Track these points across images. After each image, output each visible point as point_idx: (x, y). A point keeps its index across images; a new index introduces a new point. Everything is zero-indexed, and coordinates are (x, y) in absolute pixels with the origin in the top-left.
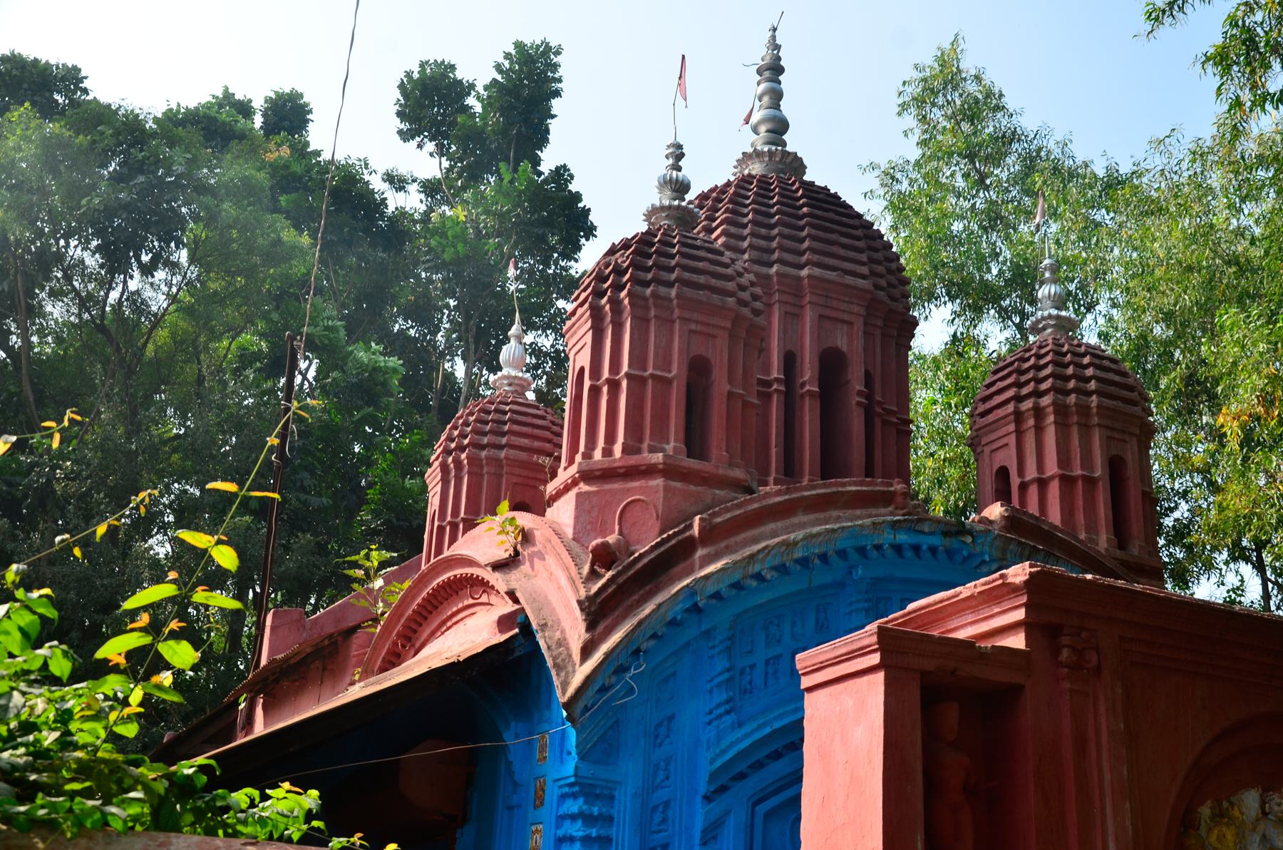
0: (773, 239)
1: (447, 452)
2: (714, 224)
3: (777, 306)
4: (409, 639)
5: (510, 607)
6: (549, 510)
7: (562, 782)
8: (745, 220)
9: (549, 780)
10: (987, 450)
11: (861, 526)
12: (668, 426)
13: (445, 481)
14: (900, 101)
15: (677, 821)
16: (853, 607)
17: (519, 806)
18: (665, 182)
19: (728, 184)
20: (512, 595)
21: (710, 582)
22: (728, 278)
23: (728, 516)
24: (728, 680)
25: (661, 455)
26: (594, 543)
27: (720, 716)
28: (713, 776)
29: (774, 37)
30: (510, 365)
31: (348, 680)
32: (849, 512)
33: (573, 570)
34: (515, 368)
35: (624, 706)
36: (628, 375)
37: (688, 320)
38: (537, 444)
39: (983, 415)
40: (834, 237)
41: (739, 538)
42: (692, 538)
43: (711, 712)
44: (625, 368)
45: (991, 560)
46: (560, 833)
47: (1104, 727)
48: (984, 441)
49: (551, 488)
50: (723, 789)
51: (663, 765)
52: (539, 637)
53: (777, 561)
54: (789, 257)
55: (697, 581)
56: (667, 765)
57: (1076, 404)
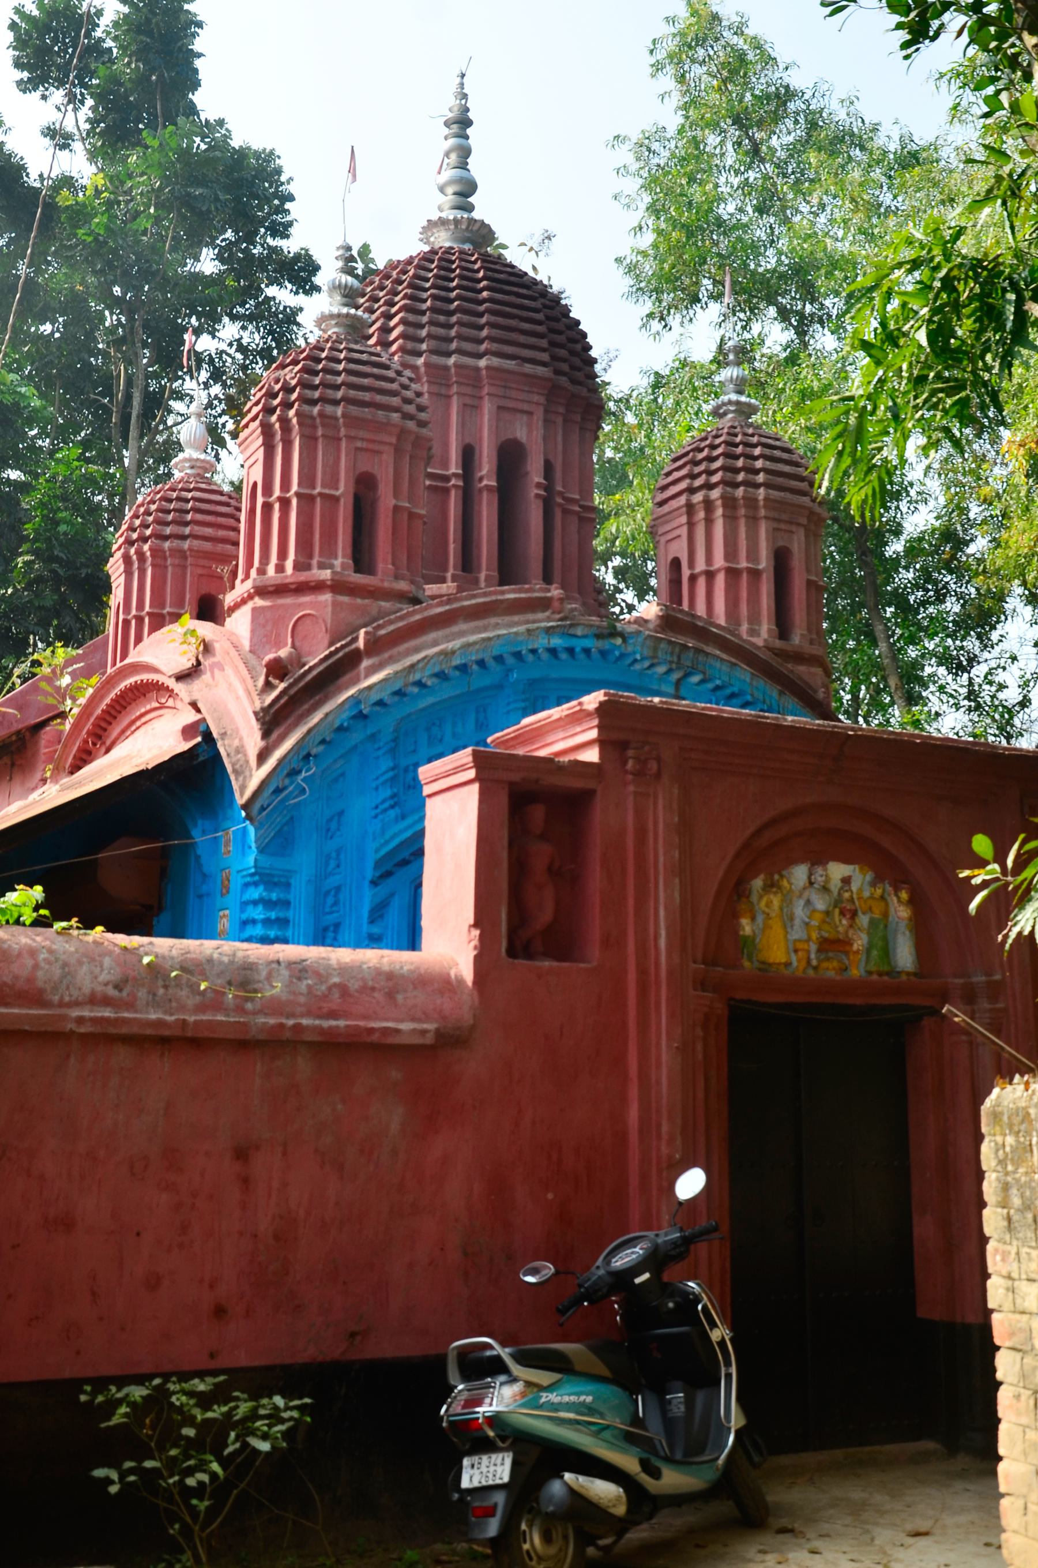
1: (130, 542)
2: (394, 310)
3: (455, 398)
4: (100, 737)
5: (192, 717)
6: (228, 620)
8: (424, 306)
10: (663, 539)
11: (516, 633)
12: (336, 542)
13: (128, 573)
14: (653, 61)
17: (208, 894)
19: (409, 261)
20: (194, 705)
21: (374, 690)
22: (394, 394)
23: (392, 628)
24: (393, 779)
25: (329, 571)
27: (385, 810)
28: (378, 864)
29: (462, 85)
31: (38, 776)
32: (507, 619)
33: (250, 682)
35: (299, 803)
36: (297, 494)
39: (661, 504)
42: (357, 650)
43: (377, 807)
44: (295, 488)
45: (643, 659)
46: (244, 917)
47: (661, 820)
48: (661, 530)
49: (230, 599)
50: (388, 874)
51: (334, 855)
53: (437, 669)
54: (468, 346)
55: (361, 691)
57: (744, 498)
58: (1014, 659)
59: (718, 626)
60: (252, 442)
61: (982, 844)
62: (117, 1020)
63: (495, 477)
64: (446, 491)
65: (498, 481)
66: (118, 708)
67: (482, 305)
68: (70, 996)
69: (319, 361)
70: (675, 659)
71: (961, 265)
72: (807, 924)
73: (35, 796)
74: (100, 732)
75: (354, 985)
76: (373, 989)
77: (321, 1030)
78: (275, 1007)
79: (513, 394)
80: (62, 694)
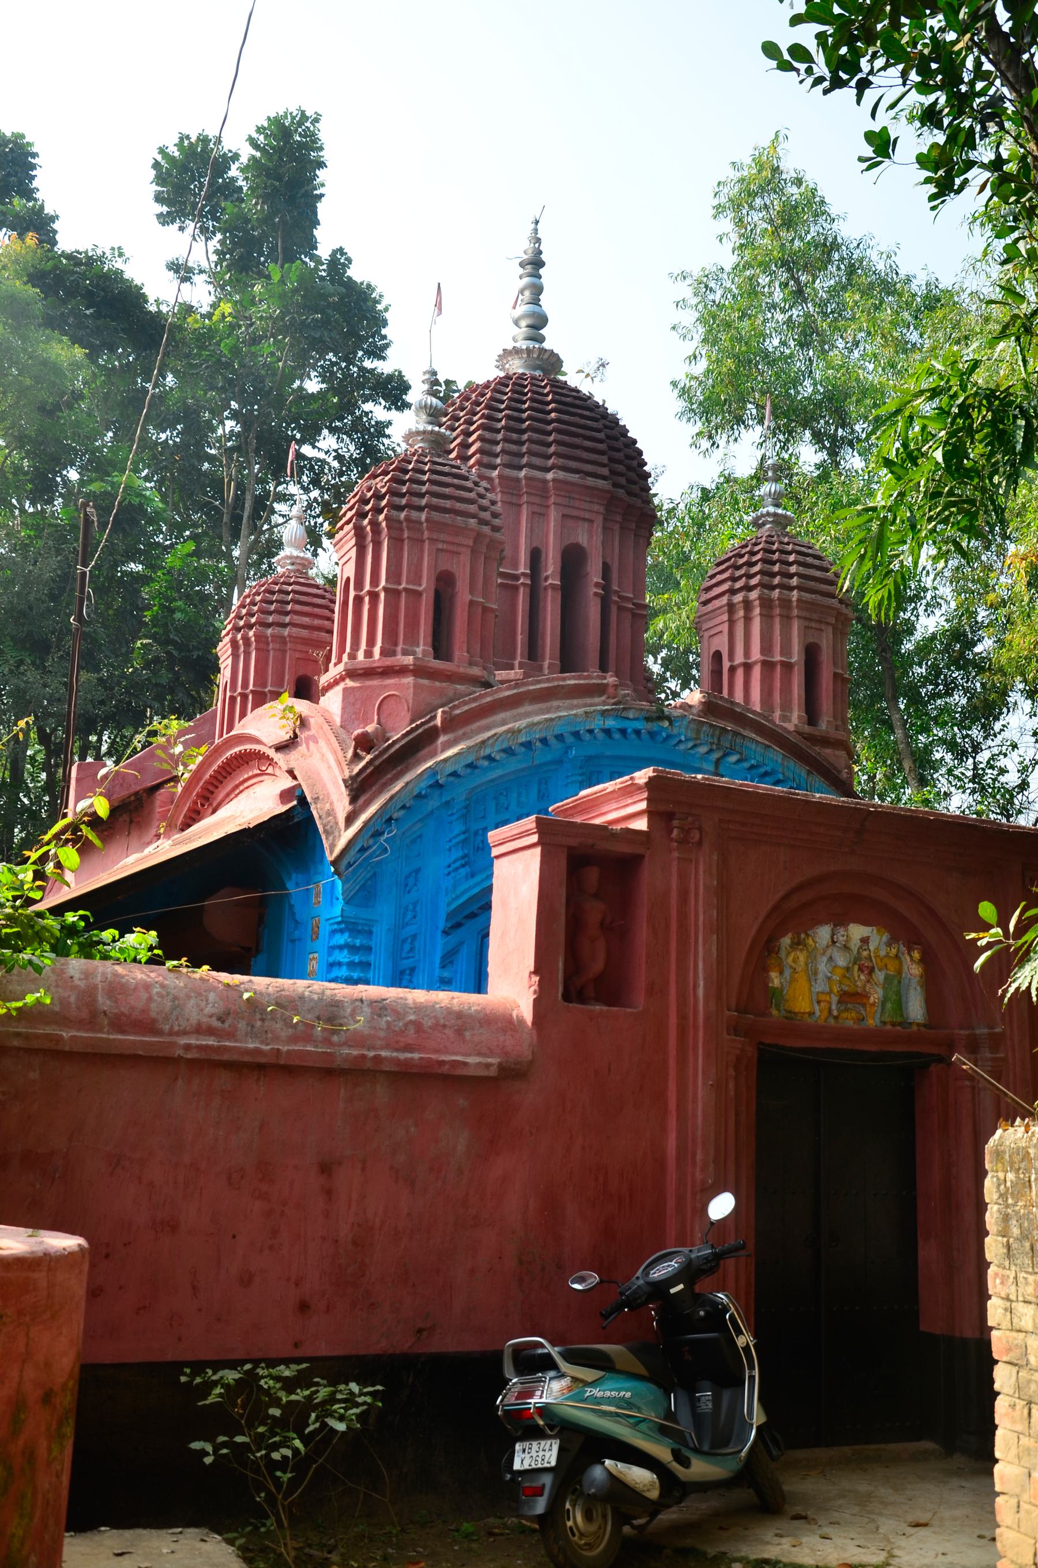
0: (523, 443)
1: (237, 629)
2: (472, 428)
3: (525, 506)
4: (207, 799)
5: (289, 783)
6: (322, 698)
7: (332, 921)
8: (499, 425)
9: (322, 919)
10: (706, 635)
11: (575, 715)
13: (235, 656)
14: (716, 202)
15: (422, 950)
16: (570, 780)
17: (300, 939)
18: (421, 408)
20: (291, 773)
21: (449, 763)
23: (466, 708)
24: (465, 841)
26: (356, 733)
27: (457, 869)
28: (450, 916)
29: (536, 230)
30: (292, 545)
31: (153, 832)
33: (340, 754)
34: (297, 547)
35: (378, 862)
36: (385, 589)
37: (437, 540)
38: (317, 622)
40: (577, 441)
41: (475, 726)
42: (435, 727)
43: (449, 866)
46: (331, 960)
47: (701, 883)
48: (705, 626)
49: (324, 680)
50: (458, 925)
51: (411, 907)
52: (312, 808)
53: (504, 746)
55: (438, 763)
56: (415, 907)
57: (779, 599)
58: (1014, 746)
59: (754, 712)
60: (346, 542)
61: (987, 910)
62: (219, 1047)
63: (559, 577)
64: (516, 588)
65: (561, 580)
66: (224, 774)
67: (551, 428)
68: (179, 1026)
69: (406, 472)
70: (716, 741)
71: (976, 394)
72: (829, 978)
73: (150, 849)
74: (208, 795)
75: (428, 1023)
76: (444, 1026)
77: (397, 1062)
78: (358, 1040)
79: (577, 504)
80: (176, 760)
